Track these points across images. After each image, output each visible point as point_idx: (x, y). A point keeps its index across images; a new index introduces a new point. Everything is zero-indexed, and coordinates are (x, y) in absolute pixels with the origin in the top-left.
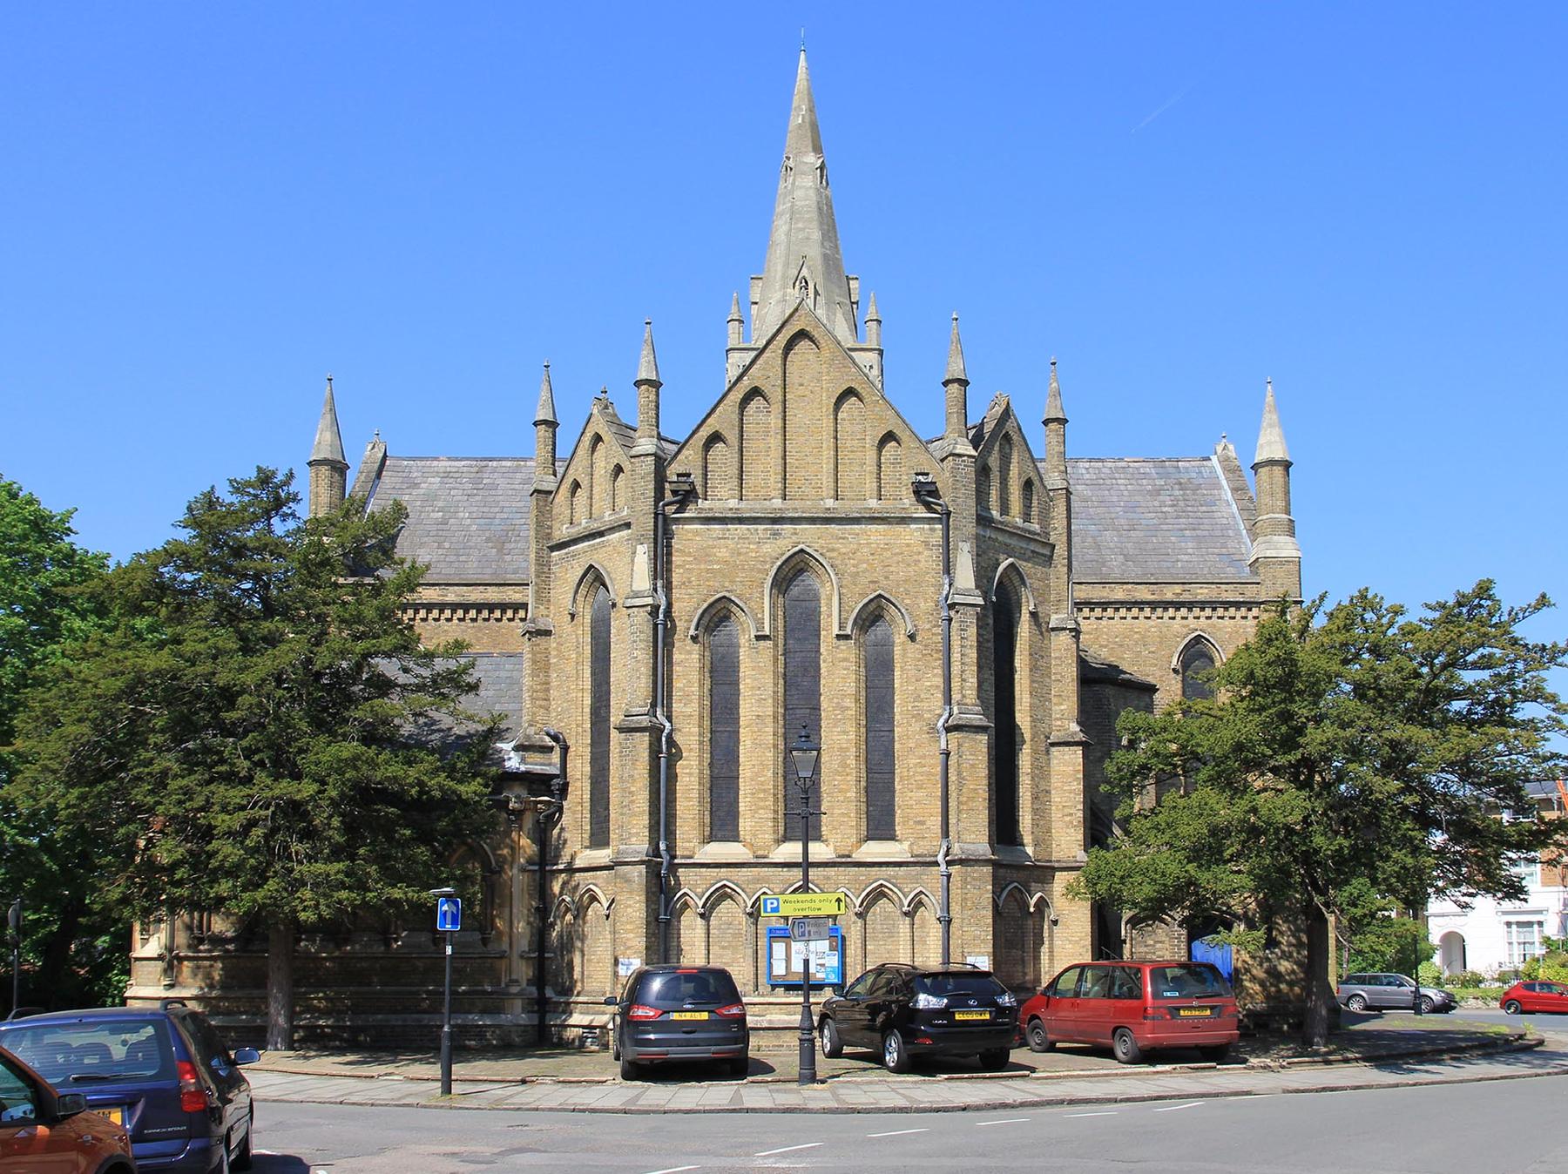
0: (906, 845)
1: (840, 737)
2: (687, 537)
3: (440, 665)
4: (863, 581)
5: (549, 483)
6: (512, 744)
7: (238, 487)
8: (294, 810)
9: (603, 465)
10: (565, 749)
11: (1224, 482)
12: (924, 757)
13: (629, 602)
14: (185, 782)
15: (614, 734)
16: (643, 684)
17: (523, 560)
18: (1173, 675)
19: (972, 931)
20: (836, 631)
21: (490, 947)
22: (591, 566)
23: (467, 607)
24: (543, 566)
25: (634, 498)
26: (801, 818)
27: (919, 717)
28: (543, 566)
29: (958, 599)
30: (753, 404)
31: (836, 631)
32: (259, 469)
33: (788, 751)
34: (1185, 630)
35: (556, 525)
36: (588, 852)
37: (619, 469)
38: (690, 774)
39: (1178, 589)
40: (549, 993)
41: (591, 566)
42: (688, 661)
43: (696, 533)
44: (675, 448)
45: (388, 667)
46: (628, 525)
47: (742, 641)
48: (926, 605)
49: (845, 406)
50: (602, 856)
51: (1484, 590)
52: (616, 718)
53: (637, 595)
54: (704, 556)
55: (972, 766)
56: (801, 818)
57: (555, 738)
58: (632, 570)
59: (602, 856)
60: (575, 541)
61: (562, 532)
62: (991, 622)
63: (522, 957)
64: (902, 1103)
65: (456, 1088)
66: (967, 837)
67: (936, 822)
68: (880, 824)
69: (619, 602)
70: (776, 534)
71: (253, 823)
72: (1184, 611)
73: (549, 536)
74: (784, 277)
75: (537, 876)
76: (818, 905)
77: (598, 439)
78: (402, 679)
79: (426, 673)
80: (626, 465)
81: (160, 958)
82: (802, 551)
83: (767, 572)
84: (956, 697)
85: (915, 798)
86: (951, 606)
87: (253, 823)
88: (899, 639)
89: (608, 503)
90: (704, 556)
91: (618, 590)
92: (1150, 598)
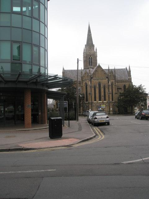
2: (92, 80)
50: (87, 102)
85: (107, 98)
91: (88, 84)
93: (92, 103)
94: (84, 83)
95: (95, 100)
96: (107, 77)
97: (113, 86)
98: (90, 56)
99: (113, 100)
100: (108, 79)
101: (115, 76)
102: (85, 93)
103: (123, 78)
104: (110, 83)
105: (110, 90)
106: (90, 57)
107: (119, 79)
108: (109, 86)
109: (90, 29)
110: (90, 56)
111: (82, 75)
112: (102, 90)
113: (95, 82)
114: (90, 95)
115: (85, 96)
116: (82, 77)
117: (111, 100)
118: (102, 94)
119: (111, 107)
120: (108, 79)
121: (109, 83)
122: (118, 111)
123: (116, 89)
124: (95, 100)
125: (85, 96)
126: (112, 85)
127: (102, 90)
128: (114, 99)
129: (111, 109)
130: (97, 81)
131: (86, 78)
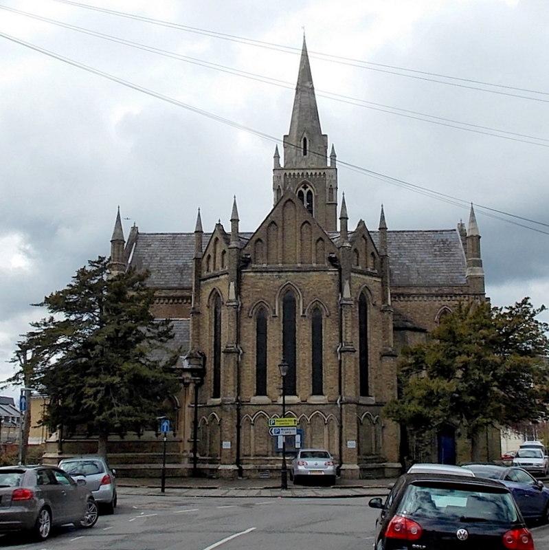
0: (326, 397)
1: (304, 355)
2: (248, 275)
3: (161, 329)
4: (311, 295)
5: (200, 256)
6: (186, 357)
7: (92, 263)
8: (110, 388)
9: (219, 251)
10: (205, 359)
11: (460, 241)
12: (332, 362)
13: (228, 304)
14: (75, 376)
15: (222, 354)
16: (233, 335)
17: (191, 281)
18: (435, 324)
19: (349, 431)
20: (301, 314)
21: (177, 437)
22: (214, 289)
23: (169, 298)
24: (198, 286)
25: (230, 264)
26: (289, 387)
27: (331, 347)
28: (198, 286)
29: (344, 302)
30: (272, 228)
31: (301, 314)
32: (100, 257)
33: (47, 491)
34: (440, 306)
35: (202, 271)
36: (213, 400)
37: (224, 252)
38: (249, 370)
39: (437, 289)
40: (198, 455)
41: (214, 289)
42: (250, 328)
43: (252, 277)
44: (247, 241)
45: (143, 329)
46: (227, 274)
47: (268, 318)
48: (333, 304)
49: (304, 226)
50: (218, 401)
51: (525, 301)
52: (223, 348)
53: (230, 301)
54: (254, 286)
55: (350, 366)
56: (289, 387)
57: (201, 354)
58: (229, 292)
59: (218, 401)
60: (209, 278)
61: (205, 274)
62: (358, 309)
63: (188, 441)
64: (315, 495)
65: (166, 490)
66: (348, 394)
67: (337, 388)
68: (317, 390)
69: (225, 303)
70: (280, 277)
71: (98, 392)
72: (439, 298)
73: (200, 276)
74: (298, 136)
75: (194, 409)
76: (288, 422)
77: (217, 239)
78: (148, 334)
79: (156, 331)
80: (227, 250)
81: (57, 441)
82: (289, 284)
83: (276, 292)
84: (344, 340)
85: (329, 379)
86: (341, 305)
87: (98, 392)
88: (324, 317)
89: (220, 265)
90: (254, 286)
91: (225, 298)
92: (426, 292)
93: (239, 404)
94: (206, 291)
95: (261, 390)
96: (333, 261)
97: (372, 312)
98: (305, 187)
99: (364, 391)
100: (340, 270)
101: (384, 257)
102: (208, 348)
103: (442, 274)
104: (347, 294)
105: (351, 336)
106: (305, 192)
107: (414, 282)
108: (341, 307)
109: (308, 63)
110: (305, 187)
111: (200, 248)
112: (304, 332)
113: (263, 285)
114: (232, 358)
115: (210, 366)
116: (198, 260)
117: (351, 391)
118: (304, 355)
119: (350, 430)
120: (340, 270)
121: (341, 290)
122: (396, 456)
123: (385, 330)
124: (261, 390)
125: (210, 366)
126: (363, 304)
127: (304, 332)
128: (372, 386)
129: (352, 444)
130: (278, 282)
131: (219, 265)
